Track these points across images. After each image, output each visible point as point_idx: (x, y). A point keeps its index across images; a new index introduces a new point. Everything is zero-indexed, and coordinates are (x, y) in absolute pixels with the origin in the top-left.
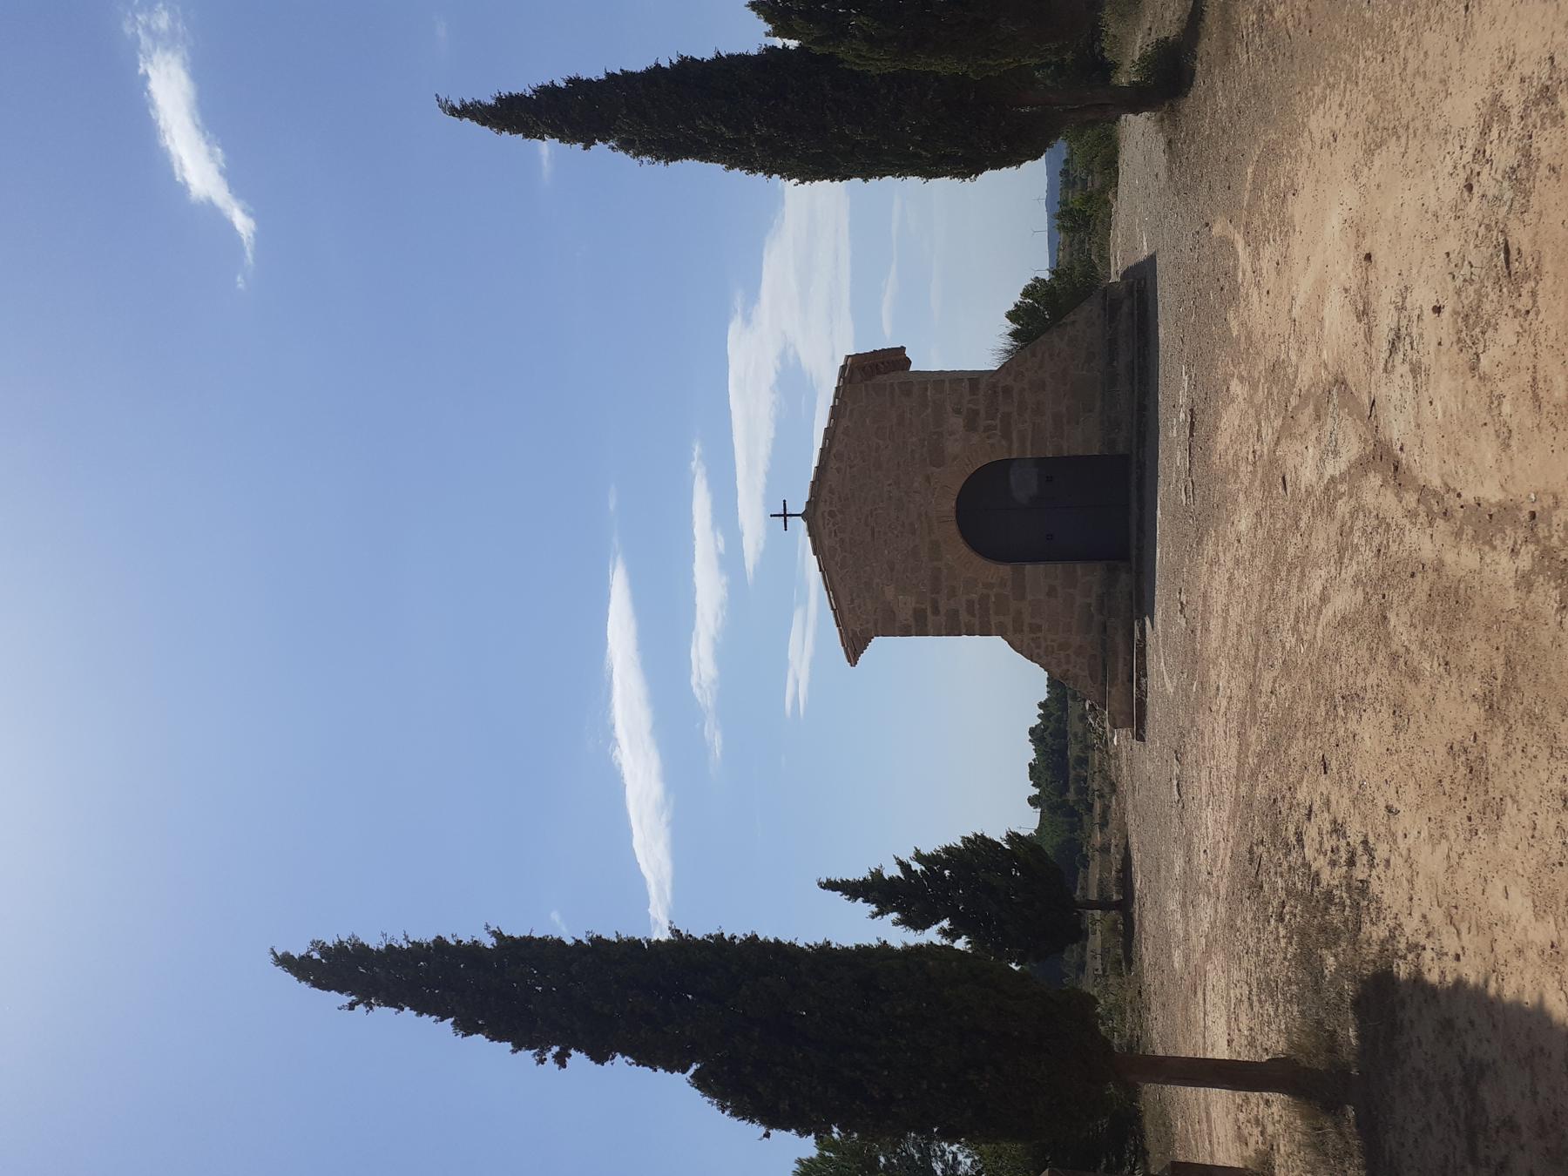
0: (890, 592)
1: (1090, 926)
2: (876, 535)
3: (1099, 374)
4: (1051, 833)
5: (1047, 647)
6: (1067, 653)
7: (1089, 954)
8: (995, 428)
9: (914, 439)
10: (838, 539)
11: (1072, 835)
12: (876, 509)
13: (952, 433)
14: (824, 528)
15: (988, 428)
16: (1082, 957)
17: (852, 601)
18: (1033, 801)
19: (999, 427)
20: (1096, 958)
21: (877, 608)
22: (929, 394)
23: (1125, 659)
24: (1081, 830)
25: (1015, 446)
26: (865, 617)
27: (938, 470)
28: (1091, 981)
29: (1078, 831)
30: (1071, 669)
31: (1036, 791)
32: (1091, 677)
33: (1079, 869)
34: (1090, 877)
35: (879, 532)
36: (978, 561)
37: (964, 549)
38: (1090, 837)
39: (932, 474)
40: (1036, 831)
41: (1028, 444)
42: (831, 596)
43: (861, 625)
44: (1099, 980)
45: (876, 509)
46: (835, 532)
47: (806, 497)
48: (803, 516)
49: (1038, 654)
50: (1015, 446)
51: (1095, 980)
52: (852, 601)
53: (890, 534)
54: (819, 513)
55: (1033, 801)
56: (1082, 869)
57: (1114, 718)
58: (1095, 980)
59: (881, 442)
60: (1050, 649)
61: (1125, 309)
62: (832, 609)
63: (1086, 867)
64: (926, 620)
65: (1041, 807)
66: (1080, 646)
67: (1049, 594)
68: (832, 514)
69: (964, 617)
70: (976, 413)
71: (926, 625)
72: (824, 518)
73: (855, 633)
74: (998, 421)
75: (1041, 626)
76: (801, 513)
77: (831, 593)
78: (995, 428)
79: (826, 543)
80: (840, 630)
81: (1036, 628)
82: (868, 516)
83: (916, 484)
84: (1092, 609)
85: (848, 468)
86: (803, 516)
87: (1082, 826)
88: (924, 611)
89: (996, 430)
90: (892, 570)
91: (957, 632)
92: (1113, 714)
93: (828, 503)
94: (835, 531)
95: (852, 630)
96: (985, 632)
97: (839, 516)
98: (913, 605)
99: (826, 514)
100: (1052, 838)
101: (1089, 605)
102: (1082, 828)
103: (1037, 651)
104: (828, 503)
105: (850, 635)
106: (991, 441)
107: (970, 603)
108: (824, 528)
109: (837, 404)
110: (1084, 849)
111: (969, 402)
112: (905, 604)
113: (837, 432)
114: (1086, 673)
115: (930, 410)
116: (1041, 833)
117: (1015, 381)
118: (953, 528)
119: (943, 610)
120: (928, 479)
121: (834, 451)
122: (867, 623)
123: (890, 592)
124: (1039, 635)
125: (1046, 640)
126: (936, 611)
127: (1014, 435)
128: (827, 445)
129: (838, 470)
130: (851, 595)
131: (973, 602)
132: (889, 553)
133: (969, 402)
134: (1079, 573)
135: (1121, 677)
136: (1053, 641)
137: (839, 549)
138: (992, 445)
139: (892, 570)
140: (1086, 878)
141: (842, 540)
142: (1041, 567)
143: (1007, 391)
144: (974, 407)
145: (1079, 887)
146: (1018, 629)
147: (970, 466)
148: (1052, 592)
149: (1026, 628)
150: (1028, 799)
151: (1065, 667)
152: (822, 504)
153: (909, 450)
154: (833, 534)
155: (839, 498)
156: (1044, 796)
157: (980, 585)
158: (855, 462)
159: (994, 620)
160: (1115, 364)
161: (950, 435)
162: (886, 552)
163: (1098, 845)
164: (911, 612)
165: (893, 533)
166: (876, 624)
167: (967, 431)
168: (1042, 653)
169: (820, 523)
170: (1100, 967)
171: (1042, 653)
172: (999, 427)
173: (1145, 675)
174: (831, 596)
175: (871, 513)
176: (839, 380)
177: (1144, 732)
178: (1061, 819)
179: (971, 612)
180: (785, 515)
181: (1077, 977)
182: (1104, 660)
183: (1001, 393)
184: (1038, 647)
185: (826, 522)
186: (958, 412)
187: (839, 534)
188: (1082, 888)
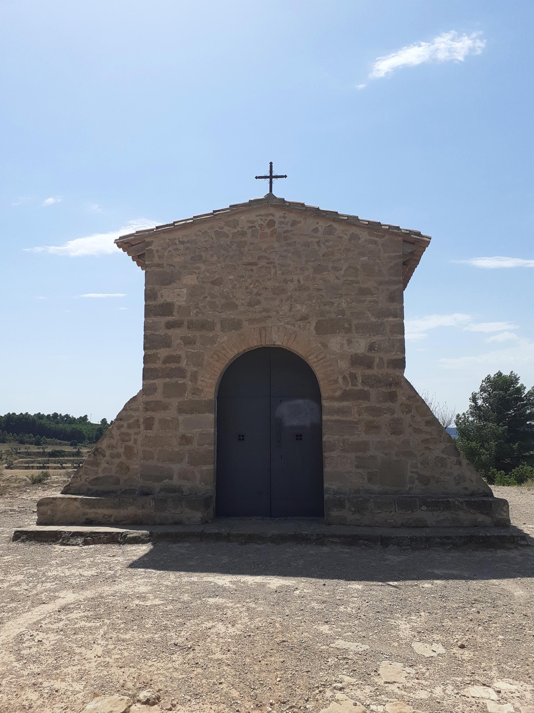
0: (190, 280)
1: (42, 447)
2: (250, 267)
3: (407, 488)
4: (88, 429)
5: (128, 435)
6: (122, 455)
7: (28, 446)
8: (354, 385)
9: (344, 305)
10: (245, 230)
11: (87, 439)
12: (275, 267)
13: (349, 342)
14: (257, 216)
15: (353, 377)
16: (27, 443)
17: (182, 243)
18: (104, 421)
19: (354, 388)
20: (25, 449)
21: (174, 266)
22: (391, 319)
23: (110, 516)
24: (89, 442)
25: (336, 404)
26: (166, 254)
27: (312, 328)
28: (15, 447)
29: (89, 441)
30: (105, 459)
31: (109, 422)
32: (96, 479)
33: (70, 442)
34: (66, 447)
35: (252, 270)
36: (220, 367)
37: (232, 353)
38: (85, 447)
39: (309, 322)
40: (89, 422)
41: (336, 417)
42: (188, 221)
43: (157, 251)
44: (14, 450)
45: (275, 267)
46: (252, 227)
47: (289, 199)
48: (270, 196)
49: (122, 426)
50: (336, 404)
51: (14, 449)
52: (182, 243)
53: (249, 281)
54: (272, 210)
55: (104, 421)
56: (70, 443)
57: (47, 504)
58: (14, 449)
59: (342, 272)
60: (128, 438)
61: (481, 518)
62: (175, 223)
63: (71, 445)
64: (161, 315)
65: (101, 425)
66: (128, 469)
67: (183, 437)
68: (271, 223)
69: (163, 353)
70: (370, 366)
71: (155, 315)
72: (267, 215)
73: (149, 244)
74: (360, 387)
75: (151, 429)
76: (274, 192)
77: (192, 221)
78: (354, 385)
79: (243, 217)
80: (153, 230)
81: (149, 424)
82: (268, 259)
83: (299, 307)
84: (167, 480)
85: (317, 240)
86: (270, 196)
87: (91, 443)
88: (171, 314)
89: (352, 385)
90: (214, 283)
91: (147, 345)
92: (52, 502)
93: (282, 220)
94: (255, 227)
95: (152, 242)
96: (147, 374)
97: (268, 231)
98: (177, 303)
99: (271, 218)
100: (85, 429)
101: (171, 478)
102: (90, 443)
103: (125, 424)
104: (282, 220)
105: (147, 240)
106: (340, 380)
107: (177, 359)
108: (257, 216)
109: (383, 227)
110: (80, 444)
111: (381, 359)
112: (178, 295)
113: (354, 228)
114: (101, 475)
115: (374, 320)
116: (89, 424)
117: (402, 404)
118: (254, 342)
119: (170, 332)
120: (304, 318)
121: (335, 225)
122: (159, 257)
123: (190, 280)
124: (142, 427)
125: (137, 434)
126: (169, 326)
127: (345, 404)
128: (341, 217)
129: (316, 230)
130: (188, 242)
131: (179, 363)
132: (230, 280)
133: (381, 359)
134: (204, 468)
135: (91, 513)
136: (136, 440)
137: (236, 231)
138: (336, 381)
139: (214, 283)
140: (66, 445)
141: (244, 234)
142: (212, 430)
143: (392, 397)
144: (375, 364)
145: (61, 441)
146: (148, 407)
147: (316, 360)
148: (185, 440)
149: (149, 414)
150: (105, 419)
151: (108, 453)
152: (281, 213)
153: (333, 300)
154: (251, 225)
155: (287, 231)
156: (106, 426)
157: (195, 369)
158: (323, 246)
159: (159, 382)
160: (424, 508)
161: (348, 340)
162: (232, 277)
163: (81, 450)
164: (169, 300)
165: (251, 284)
166: (158, 265)
167: (352, 356)
168: (123, 430)
169: (262, 212)
170: (21, 451)
171: (123, 430)
172: (354, 388)
173: (86, 543)
174: (188, 221)
175: (270, 263)
176: (406, 230)
177: (23, 541)
178: (95, 434)
179: (169, 359)
180: (271, 177)
181: (17, 440)
182: (113, 492)
183: (389, 390)
184: (129, 426)
185: (263, 218)
186: (371, 347)
187: (250, 230)
188: (60, 443)
